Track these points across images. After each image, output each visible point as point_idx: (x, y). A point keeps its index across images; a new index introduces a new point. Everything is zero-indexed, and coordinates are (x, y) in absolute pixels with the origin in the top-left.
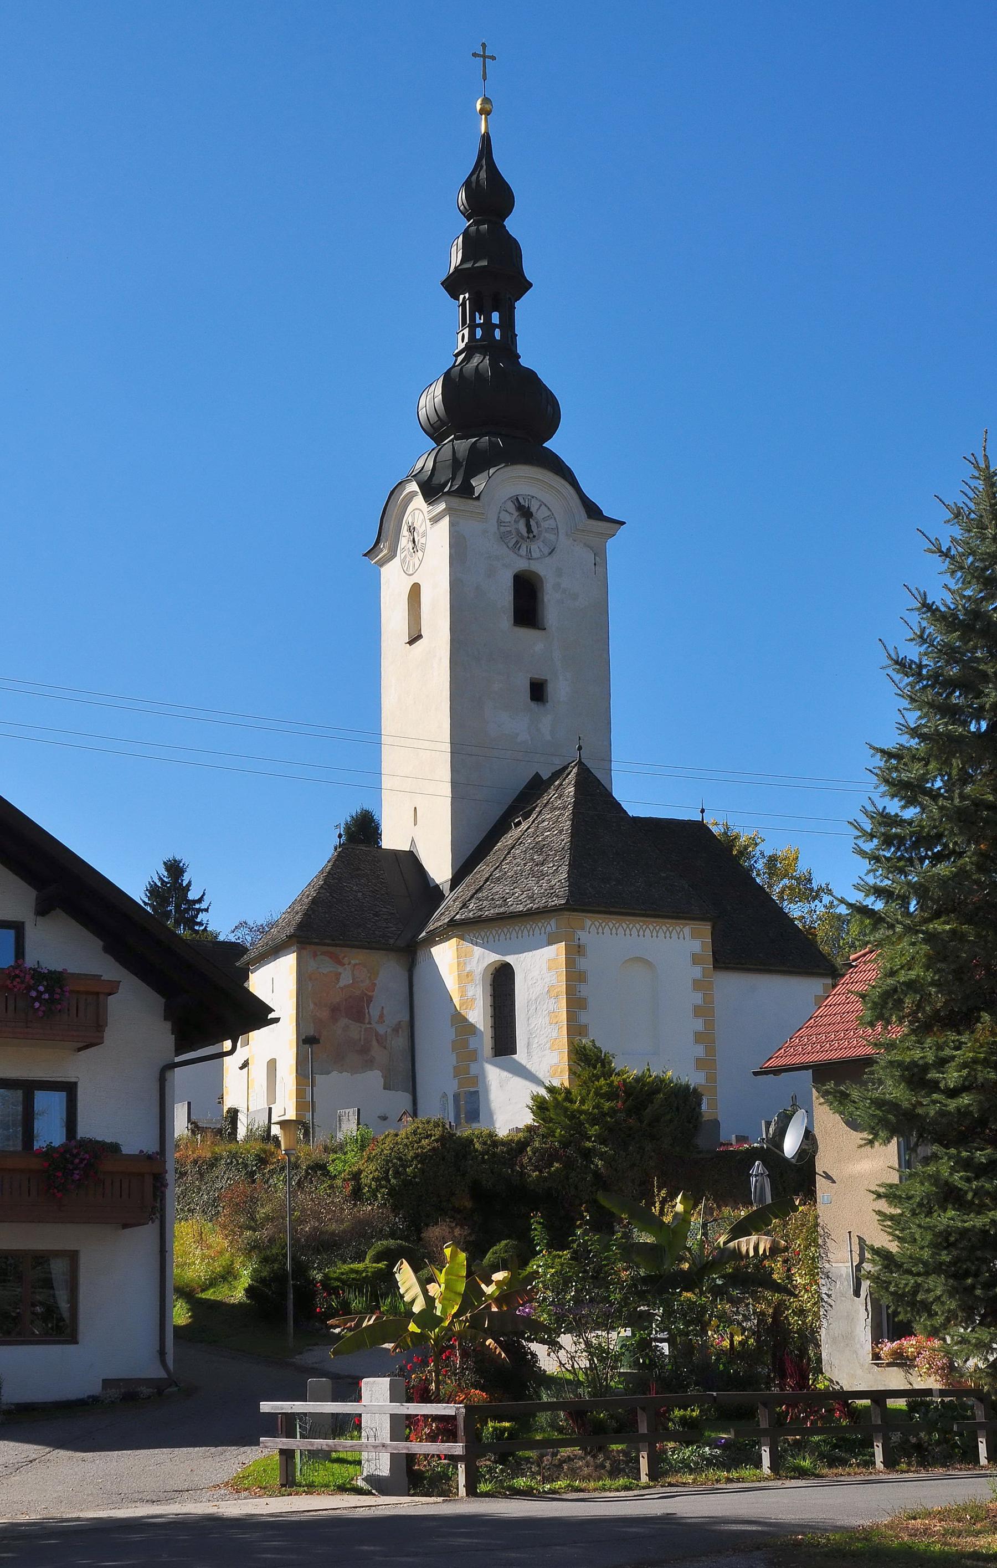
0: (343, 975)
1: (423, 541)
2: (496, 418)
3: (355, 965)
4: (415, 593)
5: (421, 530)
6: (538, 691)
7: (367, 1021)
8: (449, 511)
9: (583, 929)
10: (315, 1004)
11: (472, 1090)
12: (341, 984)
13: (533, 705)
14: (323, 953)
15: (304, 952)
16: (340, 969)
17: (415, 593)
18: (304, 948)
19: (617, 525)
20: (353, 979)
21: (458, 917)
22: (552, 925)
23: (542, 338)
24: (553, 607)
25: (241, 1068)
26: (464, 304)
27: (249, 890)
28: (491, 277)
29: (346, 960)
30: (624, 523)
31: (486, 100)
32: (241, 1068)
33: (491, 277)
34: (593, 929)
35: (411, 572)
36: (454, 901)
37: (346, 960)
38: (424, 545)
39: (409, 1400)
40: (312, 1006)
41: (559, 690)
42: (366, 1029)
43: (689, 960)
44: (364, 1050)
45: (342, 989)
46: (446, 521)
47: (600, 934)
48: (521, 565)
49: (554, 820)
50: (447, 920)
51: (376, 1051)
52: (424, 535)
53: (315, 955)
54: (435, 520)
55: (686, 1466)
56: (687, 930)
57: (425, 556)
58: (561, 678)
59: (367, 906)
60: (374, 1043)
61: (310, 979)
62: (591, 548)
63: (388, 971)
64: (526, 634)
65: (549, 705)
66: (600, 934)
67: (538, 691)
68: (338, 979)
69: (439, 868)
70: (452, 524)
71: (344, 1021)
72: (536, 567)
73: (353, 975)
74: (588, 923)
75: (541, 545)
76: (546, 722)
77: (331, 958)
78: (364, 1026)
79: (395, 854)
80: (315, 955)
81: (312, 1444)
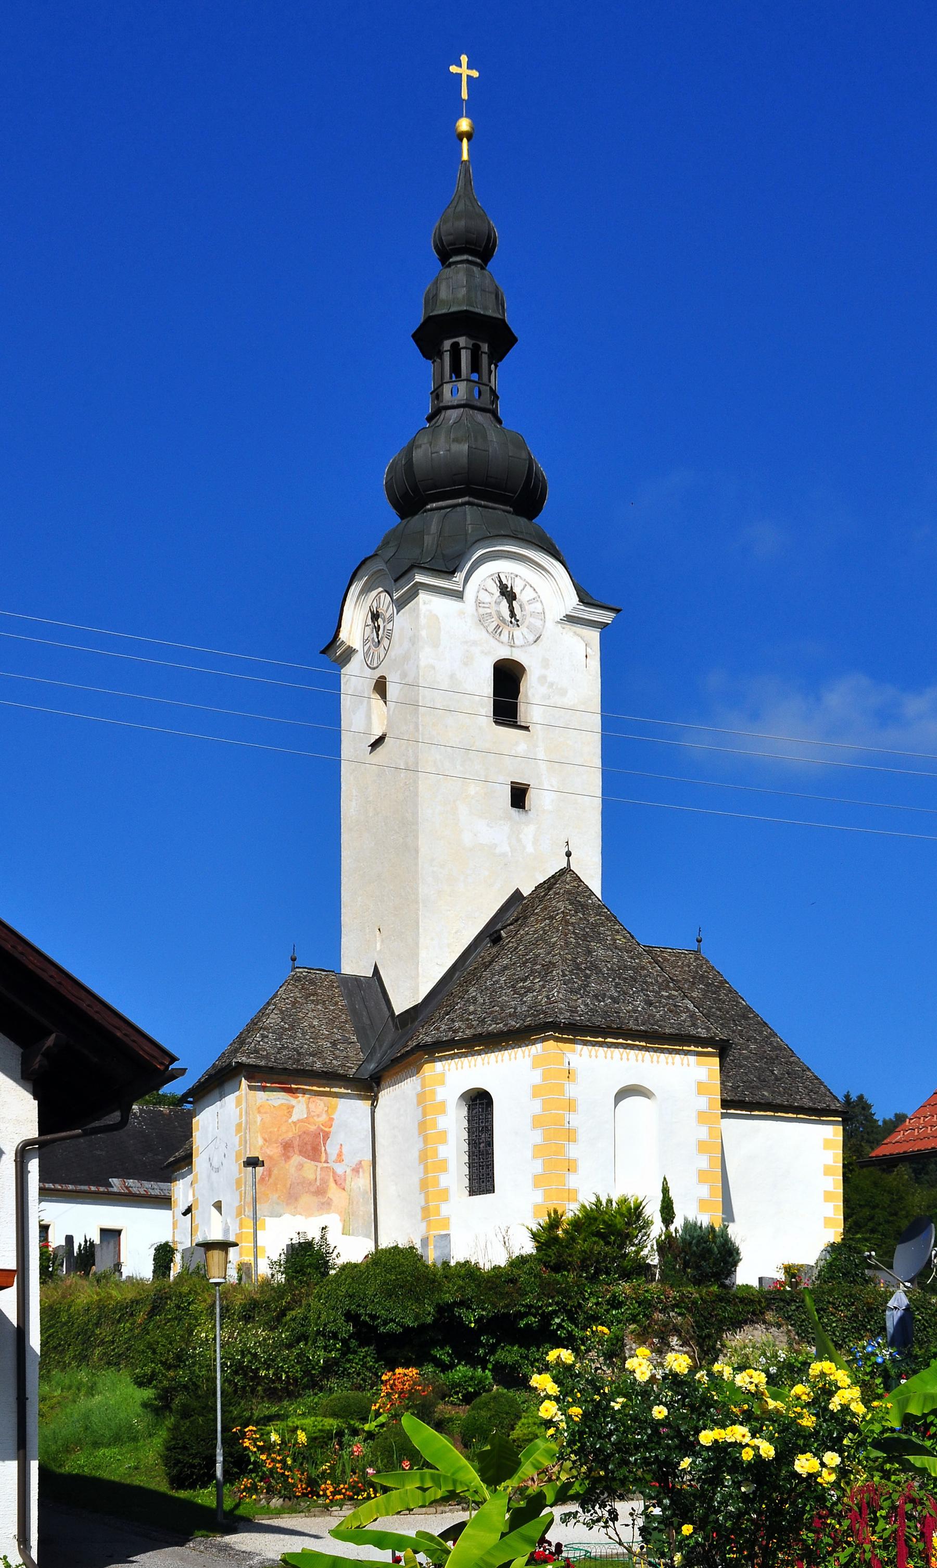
7: (323, 1159)
10: (265, 1140)
12: (294, 1118)
42: (322, 1168)
44: (320, 1192)
45: (295, 1123)
60: (332, 1184)
61: (259, 1112)
68: (290, 1114)
71: (296, 1159)
73: (308, 1107)
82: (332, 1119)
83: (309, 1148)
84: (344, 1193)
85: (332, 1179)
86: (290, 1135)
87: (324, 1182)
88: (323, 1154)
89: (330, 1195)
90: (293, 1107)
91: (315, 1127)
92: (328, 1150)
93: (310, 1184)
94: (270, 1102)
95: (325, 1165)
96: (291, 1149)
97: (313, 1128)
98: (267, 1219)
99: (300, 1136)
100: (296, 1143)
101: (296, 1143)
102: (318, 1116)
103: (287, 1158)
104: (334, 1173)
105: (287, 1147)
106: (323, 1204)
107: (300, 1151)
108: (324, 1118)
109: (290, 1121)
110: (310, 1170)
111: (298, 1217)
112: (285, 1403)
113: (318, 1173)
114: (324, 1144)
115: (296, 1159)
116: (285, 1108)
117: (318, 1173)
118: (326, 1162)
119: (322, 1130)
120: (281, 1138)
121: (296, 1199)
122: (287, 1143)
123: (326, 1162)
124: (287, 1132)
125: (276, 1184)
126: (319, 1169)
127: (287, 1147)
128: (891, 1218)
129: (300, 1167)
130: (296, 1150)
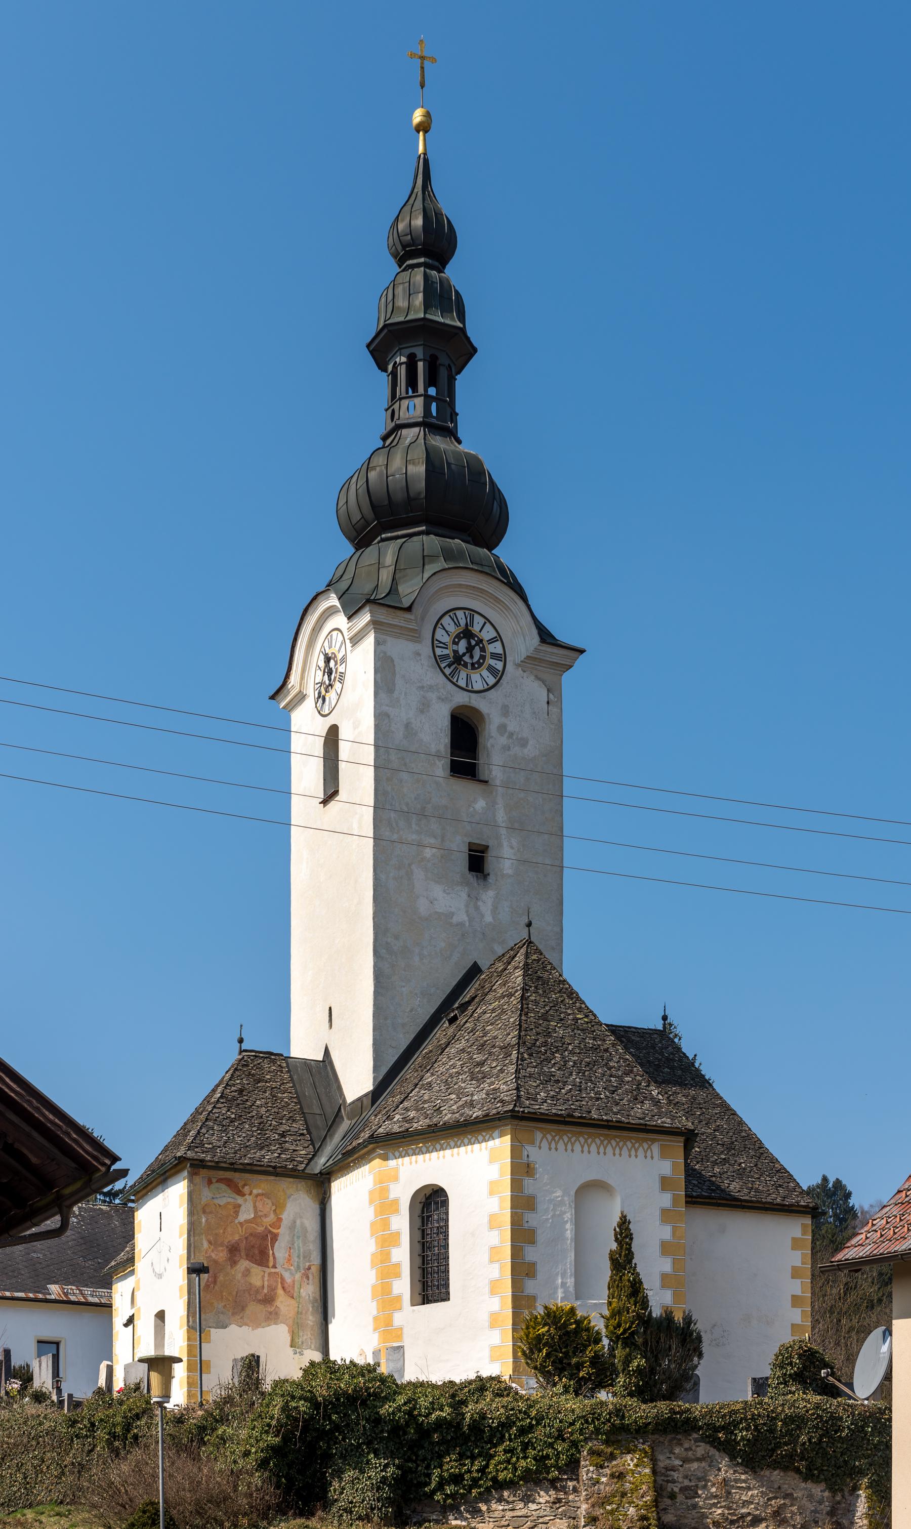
0: (243, 1208)
1: (341, 669)
2: (435, 517)
3: (257, 1196)
4: (332, 737)
5: (339, 656)
6: (477, 861)
7: (271, 1264)
8: (375, 624)
9: (532, 1143)
10: (210, 1242)
11: (395, 1344)
13: (471, 877)
14: (219, 1180)
15: (197, 1179)
16: (240, 1200)
17: (332, 737)
18: (196, 1174)
19: (578, 653)
20: (256, 1212)
21: (381, 1130)
22: (508, 1121)
23: (490, 423)
24: (495, 755)
25: (126, 1325)
26: (394, 374)
27: (127, 1094)
28: (426, 350)
29: (246, 1190)
30: (582, 651)
31: (428, 115)
32: (126, 1325)
33: (426, 350)
34: (545, 1144)
35: (327, 712)
36: (376, 1116)
37: (246, 1190)
38: (342, 675)
40: (206, 1245)
41: (505, 858)
42: (270, 1274)
43: (657, 1185)
44: (269, 1300)
45: (241, 1224)
46: (369, 642)
47: (553, 1150)
48: (462, 698)
49: (497, 1016)
50: (367, 1136)
51: (283, 1303)
52: (344, 660)
53: (210, 1182)
54: (356, 640)
56: (656, 1148)
57: (344, 685)
58: (505, 844)
59: (270, 1134)
60: (280, 1291)
61: (204, 1212)
62: (544, 682)
63: (298, 1205)
64: (463, 787)
65: (491, 879)
66: (553, 1150)
67: (477, 861)
68: (237, 1213)
69: (356, 1079)
70: (377, 643)
71: (244, 1264)
72: (476, 702)
73: (255, 1207)
74: (539, 1135)
75: (485, 673)
76: (488, 896)
77: (228, 1186)
78: (268, 1270)
79: (306, 1064)
80: (210, 1182)
82: (280, 1220)
84: (293, 1302)
86: (237, 1237)
87: (273, 1289)
88: (271, 1258)
89: (278, 1303)
90: (240, 1206)
91: (263, 1229)
92: (277, 1254)
93: (257, 1292)
94: (216, 1201)
95: (273, 1270)
97: (260, 1229)
98: (212, 1330)
99: (246, 1238)
101: (243, 1246)
103: (234, 1263)
104: (283, 1279)
105: (233, 1250)
106: (271, 1313)
107: (247, 1255)
108: (272, 1218)
109: (237, 1221)
110: (258, 1277)
113: (266, 1279)
115: (244, 1264)
116: (230, 1207)
118: (274, 1267)
119: (270, 1232)
122: (233, 1246)
123: (274, 1267)
126: (266, 1275)
127: (233, 1250)
130: (243, 1254)
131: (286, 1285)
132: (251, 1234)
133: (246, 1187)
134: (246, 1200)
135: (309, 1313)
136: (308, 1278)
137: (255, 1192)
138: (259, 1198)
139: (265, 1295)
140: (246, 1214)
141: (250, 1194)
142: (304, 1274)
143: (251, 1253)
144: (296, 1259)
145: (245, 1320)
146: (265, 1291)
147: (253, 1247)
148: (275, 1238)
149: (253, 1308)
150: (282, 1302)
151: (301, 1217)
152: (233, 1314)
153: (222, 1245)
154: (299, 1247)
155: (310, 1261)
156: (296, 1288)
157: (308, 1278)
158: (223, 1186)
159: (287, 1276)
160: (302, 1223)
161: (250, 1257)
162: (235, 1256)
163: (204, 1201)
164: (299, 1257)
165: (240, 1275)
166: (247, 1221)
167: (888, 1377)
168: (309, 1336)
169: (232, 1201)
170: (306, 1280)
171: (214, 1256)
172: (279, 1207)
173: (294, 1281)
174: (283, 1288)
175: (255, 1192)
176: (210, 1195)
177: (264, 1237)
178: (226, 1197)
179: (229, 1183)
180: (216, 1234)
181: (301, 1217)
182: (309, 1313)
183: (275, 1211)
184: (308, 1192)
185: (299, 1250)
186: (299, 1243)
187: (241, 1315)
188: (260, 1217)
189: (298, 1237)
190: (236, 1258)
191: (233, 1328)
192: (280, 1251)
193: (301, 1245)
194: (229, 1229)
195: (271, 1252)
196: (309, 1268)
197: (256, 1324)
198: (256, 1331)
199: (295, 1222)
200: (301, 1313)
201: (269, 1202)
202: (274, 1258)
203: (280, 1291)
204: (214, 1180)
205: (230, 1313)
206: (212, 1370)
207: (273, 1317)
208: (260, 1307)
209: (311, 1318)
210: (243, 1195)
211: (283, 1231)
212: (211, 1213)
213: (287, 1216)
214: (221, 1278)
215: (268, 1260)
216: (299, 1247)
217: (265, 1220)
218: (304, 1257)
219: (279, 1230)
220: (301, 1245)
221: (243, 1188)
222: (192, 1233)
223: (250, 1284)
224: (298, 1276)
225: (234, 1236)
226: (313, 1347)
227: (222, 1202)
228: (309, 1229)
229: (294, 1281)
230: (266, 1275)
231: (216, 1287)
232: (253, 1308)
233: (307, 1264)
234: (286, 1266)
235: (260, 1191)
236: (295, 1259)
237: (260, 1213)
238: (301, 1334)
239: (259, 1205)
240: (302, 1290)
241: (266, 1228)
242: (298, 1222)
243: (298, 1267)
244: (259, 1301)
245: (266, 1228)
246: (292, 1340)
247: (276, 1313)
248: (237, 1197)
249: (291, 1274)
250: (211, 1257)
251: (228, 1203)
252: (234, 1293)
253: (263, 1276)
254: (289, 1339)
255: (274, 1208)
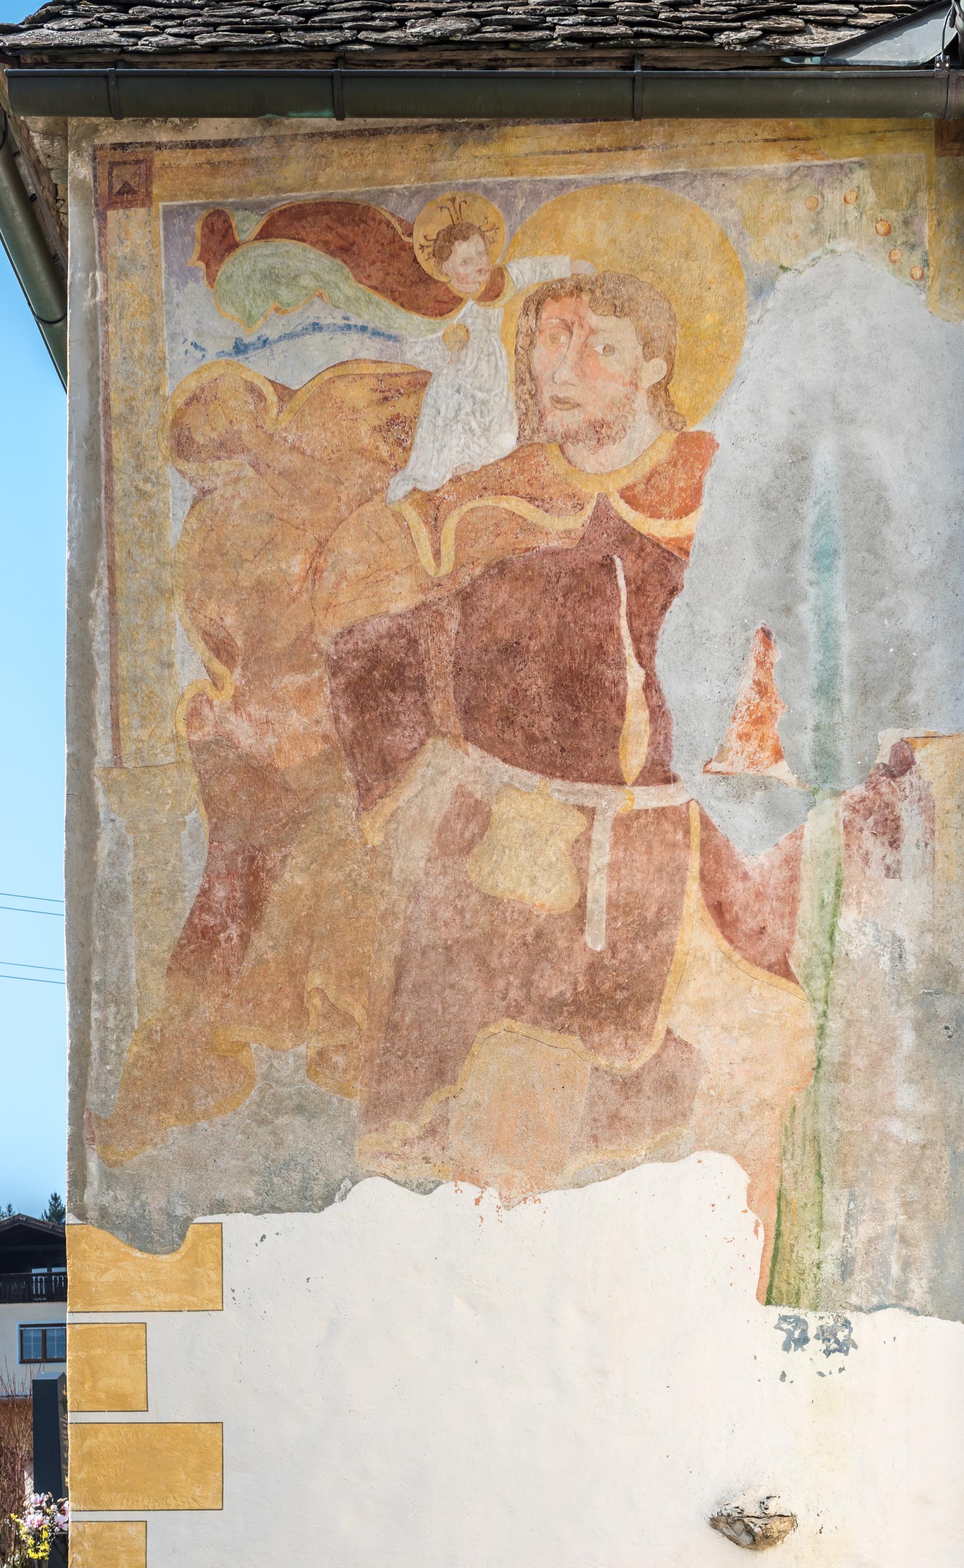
0: (440, 395)
7: (634, 757)
10: (221, 648)
12: (437, 458)
14: (285, 222)
16: (420, 340)
29: (464, 265)
37: (464, 265)
39: (212, 1213)
40: (190, 666)
42: (625, 825)
44: (615, 998)
45: (431, 505)
51: (716, 1009)
55: (721, 1531)
60: (696, 935)
61: (182, 446)
68: (399, 431)
71: (448, 769)
73: (526, 378)
77: (343, 251)
78: (613, 802)
80: (219, 240)
81: (13, 211)
82: (694, 449)
83: (535, 680)
84: (784, 999)
85: (693, 898)
86: (401, 598)
87: (645, 924)
88: (637, 718)
89: (679, 1013)
90: (419, 381)
91: (577, 522)
92: (673, 689)
93: (539, 946)
94: (259, 368)
95: (649, 798)
96: (404, 705)
97: (560, 528)
98: (239, 1227)
99: (466, 598)
100: (441, 648)
101: (441, 648)
102: (599, 431)
103: (377, 767)
104: (715, 854)
105: (378, 684)
106: (628, 1085)
107: (469, 712)
108: (642, 442)
109: (398, 488)
110: (543, 846)
111: (454, 1197)
112: (26, 1503)
113: (601, 856)
114: (645, 641)
115: (448, 769)
116: (357, 394)
117: (601, 856)
118: (659, 773)
119: (628, 537)
120: (333, 625)
121: (442, 1071)
122: (374, 659)
123: (659, 773)
124: (374, 577)
125: (295, 971)
126: (602, 834)
127: (378, 684)
128: (676, 553)
129: (470, 825)
130: (444, 702)
131: (737, 892)
132: (501, 568)
133: (462, 249)
134: (462, 339)
135: (897, 1066)
136: (891, 831)
137: (524, 273)
138: (551, 312)
139: (595, 967)
140: (465, 432)
141: (492, 292)
142: (861, 808)
143: (500, 695)
144: (810, 710)
145: (456, 1142)
146: (595, 939)
147: (511, 650)
148: (661, 572)
149: (514, 1062)
150: (705, 1006)
151: (844, 419)
152: (378, 1109)
153: (299, 654)
154: (828, 627)
155: (904, 717)
156: (807, 910)
157: (891, 831)
158: (304, 259)
159: (754, 847)
160: (852, 463)
161: (491, 721)
162: (389, 721)
163: (181, 378)
164: (826, 691)
165: (421, 847)
166: (469, 483)
167: (52, 325)
168: (895, 1216)
169: (368, 349)
170: (877, 848)
171: (244, 733)
172: (684, 361)
173: (791, 861)
174: (719, 911)
175: (524, 273)
176: (222, 329)
177: (584, 580)
178: (313, 325)
179: (346, 228)
180: (261, 589)
181: (844, 419)
182: (897, 1066)
183: (661, 390)
184: (897, 236)
185: (829, 647)
186: (827, 597)
187: (429, 1110)
188: (563, 441)
189: (824, 559)
190: (398, 740)
191: (376, 1201)
192: (691, 666)
193: (841, 613)
194: (348, 547)
195: (634, 676)
196: (902, 765)
197: (531, 1161)
198: (527, 1213)
199: (799, 455)
200: (841, 1073)
201: (620, 332)
202: (658, 713)
203: (696, 935)
204: (246, 226)
205: (356, 1103)
206: (235, 1482)
207: (646, 1109)
208: (560, 1051)
209: (906, 1097)
210: (442, 304)
211: (718, 535)
212: (225, 447)
213: (744, 422)
214: (293, 876)
215: (612, 734)
216: (828, 627)
217: (589, 459)
218: (867, 690)
219: (689, 524)
220: (841, 613)
221: (441, 252)
222: (98, 597)
223: (491, 901)
224: (822, 824)
225: (386, 582)
226: (918, 1289)
227: (300, 364)
228: (902, 497)
229: (791, 861)
230: (602, 834)
231: (261, 942)
232: (514, 1062)
233: (889, 737)
234: (737, 764)
235: (560, 267)
236: (799, 706)
237: (559, 420)
238: (836, 1211)
239: (555, 363)
240: (848, 919)
241: (602, 514)
242: (825, 455)
243: (825, 764)
244: (554, 1013)
245: (602, 514)
246: (776, 1256)
247: (670, 1086)
248: (404, 321)
249: (776, 812)
250: (225, 741)
251: (341, 369)
252: (386, 971)
253: (583, 843)
254: (754, 1248)
255: (654, 371)
